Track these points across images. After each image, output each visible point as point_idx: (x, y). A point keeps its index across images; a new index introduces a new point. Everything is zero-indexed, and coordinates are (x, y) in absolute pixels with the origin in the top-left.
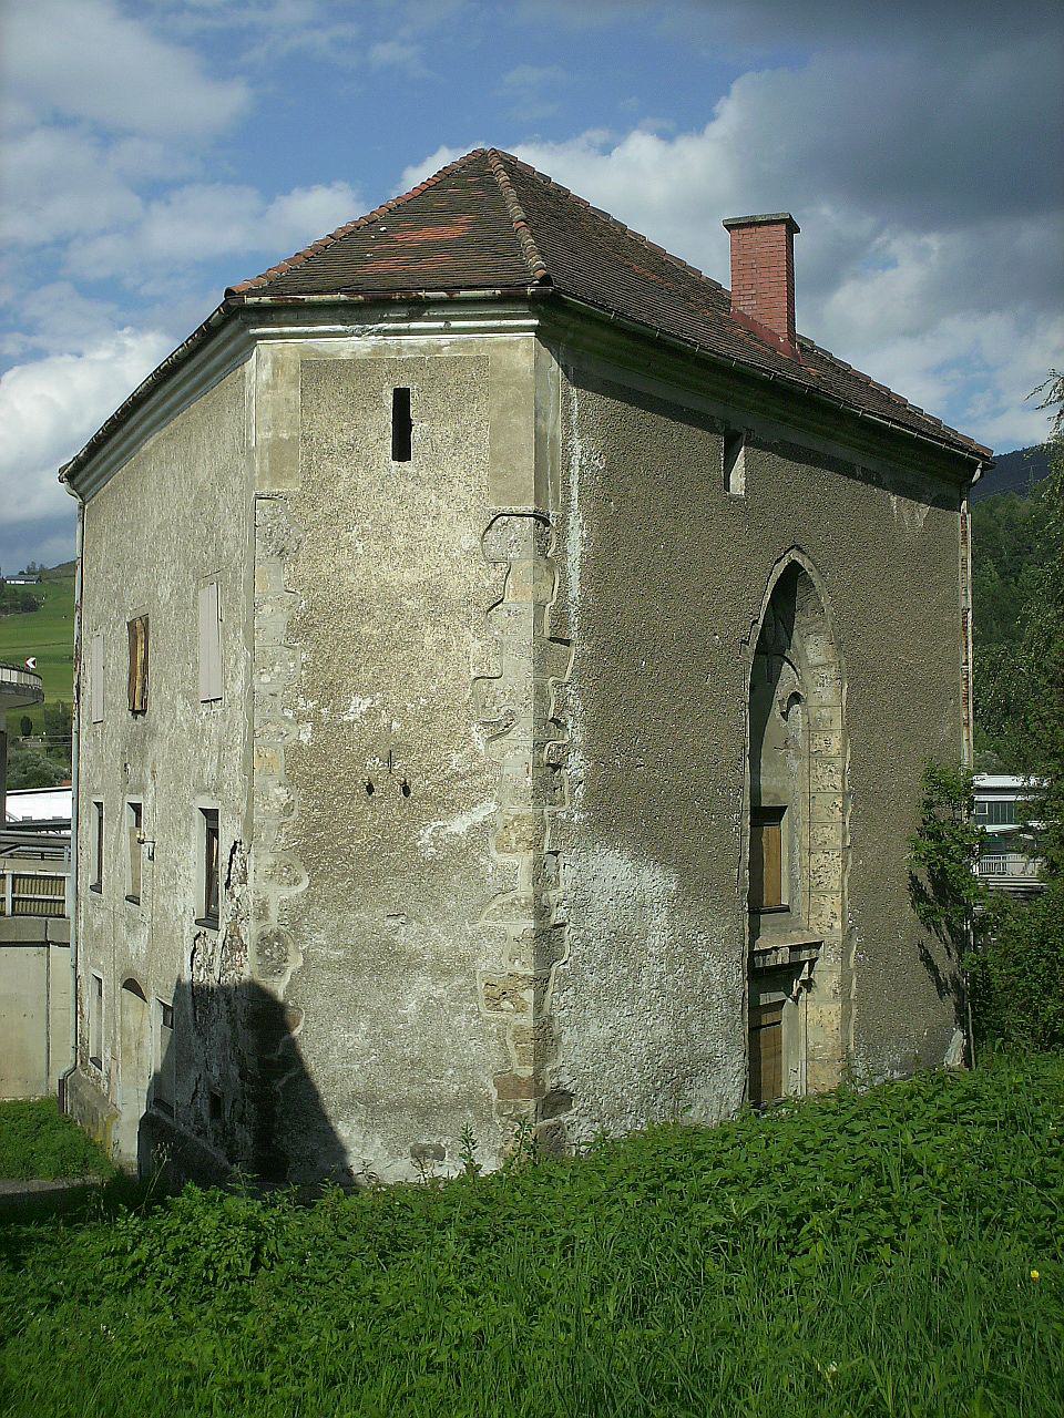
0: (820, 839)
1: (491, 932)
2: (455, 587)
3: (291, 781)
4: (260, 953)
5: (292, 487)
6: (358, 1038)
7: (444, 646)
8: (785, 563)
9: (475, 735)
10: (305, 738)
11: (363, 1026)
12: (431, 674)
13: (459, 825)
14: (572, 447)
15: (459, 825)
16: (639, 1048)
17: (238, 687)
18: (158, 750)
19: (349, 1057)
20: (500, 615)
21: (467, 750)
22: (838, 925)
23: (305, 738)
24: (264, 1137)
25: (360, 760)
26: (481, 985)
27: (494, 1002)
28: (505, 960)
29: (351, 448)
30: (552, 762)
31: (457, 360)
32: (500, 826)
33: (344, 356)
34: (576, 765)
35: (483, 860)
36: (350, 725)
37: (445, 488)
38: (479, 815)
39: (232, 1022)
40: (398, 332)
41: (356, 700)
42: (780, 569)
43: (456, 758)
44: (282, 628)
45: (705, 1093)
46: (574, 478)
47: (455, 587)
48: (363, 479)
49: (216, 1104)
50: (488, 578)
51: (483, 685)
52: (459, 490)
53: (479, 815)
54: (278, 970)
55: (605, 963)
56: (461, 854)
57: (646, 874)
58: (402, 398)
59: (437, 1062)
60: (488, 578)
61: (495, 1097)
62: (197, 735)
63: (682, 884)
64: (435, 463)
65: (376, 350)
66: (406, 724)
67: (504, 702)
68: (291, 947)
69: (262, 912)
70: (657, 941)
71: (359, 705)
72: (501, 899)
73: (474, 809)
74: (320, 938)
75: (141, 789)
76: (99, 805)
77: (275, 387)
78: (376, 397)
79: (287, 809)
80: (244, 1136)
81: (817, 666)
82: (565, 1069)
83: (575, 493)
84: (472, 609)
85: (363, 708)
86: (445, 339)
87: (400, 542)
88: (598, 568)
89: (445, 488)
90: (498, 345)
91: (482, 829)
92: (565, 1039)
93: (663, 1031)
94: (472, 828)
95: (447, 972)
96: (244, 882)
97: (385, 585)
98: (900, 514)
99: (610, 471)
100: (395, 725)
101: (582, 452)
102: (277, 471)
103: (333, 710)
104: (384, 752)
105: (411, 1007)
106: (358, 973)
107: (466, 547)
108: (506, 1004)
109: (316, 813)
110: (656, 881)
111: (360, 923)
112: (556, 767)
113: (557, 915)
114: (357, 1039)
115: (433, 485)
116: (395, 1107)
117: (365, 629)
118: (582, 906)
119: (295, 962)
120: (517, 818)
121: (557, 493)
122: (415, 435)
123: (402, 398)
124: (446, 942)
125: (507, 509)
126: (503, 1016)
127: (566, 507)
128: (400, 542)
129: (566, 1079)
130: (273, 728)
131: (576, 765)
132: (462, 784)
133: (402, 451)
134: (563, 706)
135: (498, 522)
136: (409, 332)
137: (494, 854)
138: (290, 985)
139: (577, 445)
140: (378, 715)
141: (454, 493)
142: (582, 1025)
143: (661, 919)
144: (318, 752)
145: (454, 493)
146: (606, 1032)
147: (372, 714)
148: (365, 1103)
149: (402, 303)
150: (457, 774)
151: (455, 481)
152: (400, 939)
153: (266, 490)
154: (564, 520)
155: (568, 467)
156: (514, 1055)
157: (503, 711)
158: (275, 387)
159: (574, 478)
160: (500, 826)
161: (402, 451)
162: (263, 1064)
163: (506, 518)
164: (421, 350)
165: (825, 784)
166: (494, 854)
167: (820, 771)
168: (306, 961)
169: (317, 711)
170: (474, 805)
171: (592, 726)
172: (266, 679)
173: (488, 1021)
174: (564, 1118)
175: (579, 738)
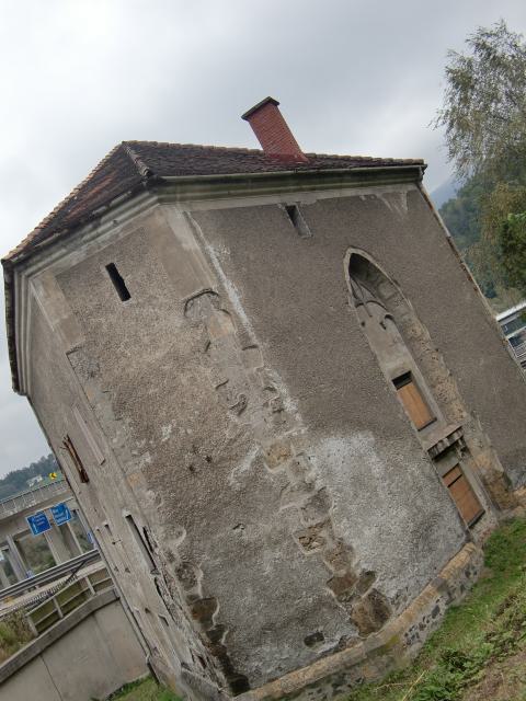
0: (435, 379)
1: (288, 510)
2: (184, 348)
3: (152, 487)
4: (180, 578)
5: (81, 340)
6: (249, 599)
7: (193, 379)
10: (148, 460)
11: (249, 591)
12: (193, 397)
13: (246, 465)
15: (246, 465)
16: (396, 529)
17: (107, 451)
18: (100, 495)
19: (250, 610)
20: (213, 348)
22: (465, 414)
23: (148, 460)
24: (228, 671)
25: (180, 458)
26: (297, 541)
27: (307, 545)
28: (302, 522)
29: (99, 307)
31: (128, 238)
32: (265, 454)
33: (74, 263)
34: (290, 405)
35: (266, 477)
36: (167, 442)
37: (154, 302)
38: (253, 455)
39: (187, 618)
40: (93, 238)
41: (164, 428)
42: (347, 260)
43: (227, 432)
44: (110, 411)
45: (442, 532)
46: (216, 264)
47: (184, 348)
48: (113, 318)
49: (201, 659)
51: (222, 389)
52: (162, 299)
54: (193, 583)
55: (356, 495)
56: (253, 479)
57: (355, 441)
58: (112, 269)
59: (296, 590)
61: (333, 595)
62: (107, 480)
63: (375, 435)
64: (144, 292)
65: (88, 252)
66: (192, 427)
68: (194, 569)
69: (171, 558)
70: (377, 469)
71: (167, 430)
72: (285, 492)
74: (206, 557)
75: (104, 519)
76: (107, 526)
77: (49, 296)
78: (99, 275)
79: (158, 501)
80: (220, 674)
82: (360, 563)
83: (221, 272)
84: (198, 355)
85: (169, 431)
86: (118, 229)
87: (146, 340)
88: (252, 305)
89: (154, 302)
90: (145, 218)
91: (258, 461)
92: (354, 546)
93: (404, 513)
95: (277, 543)
96: (156, 546)
97: (149, 365)
98: (395, 209)
99: (234, 255)
100: (189, 431)
102: (70, 336)
103: (155, 440)
104: (189, 447)
105: (268, 569)
106: (233, 566)
107: (179, 325)
108: (315, 544)
109: (173, 495)
110: (362, 441)
111: (221, 540)
112: (279, 411)
113: (319, 485)
114: (249, 599)
116: (286, 625)
117: (151, 392)
118: (329, 474)
119: (200, 576)
120: (272, 447)
122: (127, 284)
123: (112, 269)
124: (268, 528)
125: (189, 296)
126: (316, 550)
127: (219, 280)
128: (146, 340)
129: (364, 566)
130: (130, 463)
131: (290, 405)
133: (125, 295)
134: (267, 378)
135: (189, 305)
136: (99, 235)
137: (270, 471)
138: (203, 588)
139: (210, 248)
140: (178, 430)
142: (360, 534)
143: (374, 458)
144: (156, 464)
146: (374, 530)
147: (175, 431)
148: (270, 629)
149: (87, 222)
152: (245, 538)
153: (70, 348)
154: (222, 288)
155: (210, 261)
156: (332, 568)
158: (49, 296)
159: (216, 264)
160: (265, 454)
161: (125, 295)
162: (208, 634)
164: (110, 240)
166: (270, 471)
167: (418, 346)
168: (204, 572)
169: (147, 444)
171: (288, 381)
172: (115, 441)
173: (310, 557)
174: (375, 585)
175: (284, 391)
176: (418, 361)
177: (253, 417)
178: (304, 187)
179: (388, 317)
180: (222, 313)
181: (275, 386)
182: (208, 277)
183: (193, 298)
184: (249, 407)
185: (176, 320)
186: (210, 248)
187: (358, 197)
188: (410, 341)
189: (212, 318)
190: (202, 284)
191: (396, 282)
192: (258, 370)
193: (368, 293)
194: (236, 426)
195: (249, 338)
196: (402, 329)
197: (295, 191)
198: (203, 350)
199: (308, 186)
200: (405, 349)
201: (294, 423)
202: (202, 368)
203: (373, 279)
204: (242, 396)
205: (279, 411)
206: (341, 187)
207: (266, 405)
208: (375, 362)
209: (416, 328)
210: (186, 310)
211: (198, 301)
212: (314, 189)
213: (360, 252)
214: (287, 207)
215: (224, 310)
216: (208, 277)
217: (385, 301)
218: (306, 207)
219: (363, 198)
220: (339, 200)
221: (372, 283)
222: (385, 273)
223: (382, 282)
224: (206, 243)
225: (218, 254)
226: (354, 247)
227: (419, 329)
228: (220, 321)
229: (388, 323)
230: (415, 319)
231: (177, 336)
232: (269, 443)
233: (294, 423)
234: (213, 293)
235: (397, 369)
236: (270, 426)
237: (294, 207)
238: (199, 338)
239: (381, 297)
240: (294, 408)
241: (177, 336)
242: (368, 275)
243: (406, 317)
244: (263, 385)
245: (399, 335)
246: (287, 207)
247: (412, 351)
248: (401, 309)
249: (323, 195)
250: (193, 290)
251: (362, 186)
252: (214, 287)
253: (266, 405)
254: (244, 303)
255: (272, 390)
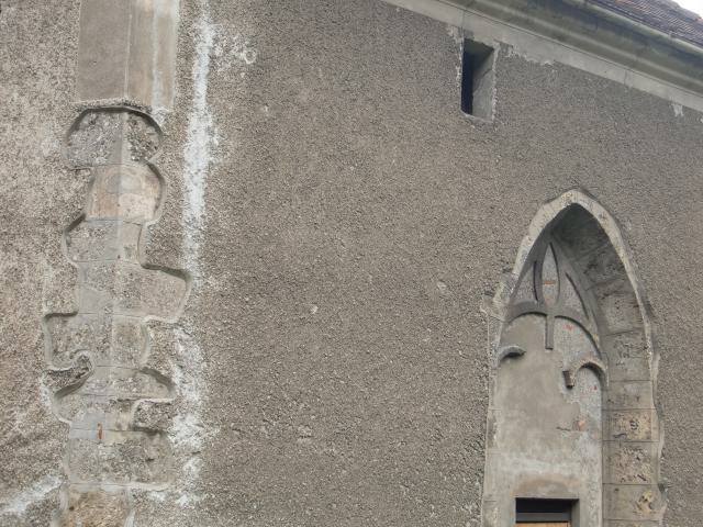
8: (559, 206)
9: (43, 388)
14: (197, 33)
20: (82, 236)
21: (32, 407)
30: (140, 424)
32: (64, 505)
34: (186, 431)
37: (29, 82)
38: (41, 492)
42: (549, 212)
43: (20, 417)
46: (200, 69)
50: (68, 190)
51: (57, 325)
52: (43, 84)
53: (41, 492)
60: (68, 190)
67: (78, 346)
73: (36, 485)
81: (619, 334)
83: (201, 87)
84: (49, 230)
88: (229, 187)
89: (29, 82)
94: (33, 509)
99: (258, 72)
101: (216, 40)
107: (46, 153)
112: (151, 432)
115: (15, 80)
120: (84, 497)
121: (169, 86)
125: (93, 102)
127: (185, 103)
132: (24, 451)
135: (85, 122)
139: (207, 32)
141: (38, 88)
145: (38, 88)
150: (19, 437)
151: (40, 73)
154: (180, 120)
155: (188, 54)
157: (76, 357)
159: (200, 69)
160: (64, 505)
163: (94, 116)
165: (631, 474)
167: (625, 458)
170: (36, 478)
171: (219, 382)
176: (611, 489)
177: (80, 415)
178: (536, 20)
179: (592, 367)
180: (142, 170)
181: (177, 377)
182: (157, 85)
183: (99, 110)
184: (84, 389)
185: (47, 139)
186: (207, 32)
187: (666, 104)
188: (614, 440)
189: (112, 171)
190: (133, 89)
191: (649, 307)
192: (155, 325)
193: (572, 302)
194: (42, 412)
195: (176, 250)
196: (611, 410)
197: (511, 19)
198: (63, 224)
199: (552, 27)
200: (593, 451)
201: (173, 472)
202: (42, 261)
203: (600, 278)
204: (85, 360)
205: (151, 432)
206: (633, 65)
207: (124, 404)
208: (480, 440)
209: (642, 422)
210: (76, 127)
211: (106, 121)
212: (562, 38)
213: (596, 211)
214: (468, 43)
215: (152, 167)
216: (157, 85)
217: (608, 335)
218: (519, 64)
219: (678, 111)
220: (614, 87)
221: (595, 285)
222: (632, 279)
223: (616, 292)
224: (205, 16)
225: (218, 52)
226: (585, 192)
227: (647, 425)
228: (126, 183)
229: (589, 379)
230: (649, 402)
231: (33, 171)
232: (84, 485)
233: (173, 472)
234: (150, 121)
235: (546, 483)
236: (104, 452)
237: (491, 50)
238: (67, 196)
239: (600, 321)
240: (195, 443)
241: (33, 171)
242: (593, 265)
243: (631, 388)
244: (144, 362)
245: (597, 417)
246: (468, 43)
247: (608, 461)
248: (632, 367)
249: (577, 60)
250: (108, 94)
251: (689, 86)
252: (158, 111)
253: (124, 404)
254: (216, 179)
255: (165, 381)
